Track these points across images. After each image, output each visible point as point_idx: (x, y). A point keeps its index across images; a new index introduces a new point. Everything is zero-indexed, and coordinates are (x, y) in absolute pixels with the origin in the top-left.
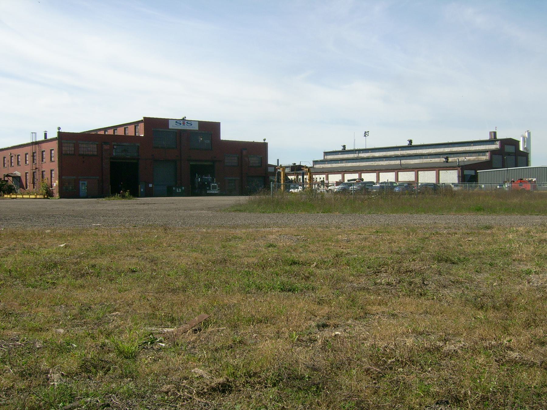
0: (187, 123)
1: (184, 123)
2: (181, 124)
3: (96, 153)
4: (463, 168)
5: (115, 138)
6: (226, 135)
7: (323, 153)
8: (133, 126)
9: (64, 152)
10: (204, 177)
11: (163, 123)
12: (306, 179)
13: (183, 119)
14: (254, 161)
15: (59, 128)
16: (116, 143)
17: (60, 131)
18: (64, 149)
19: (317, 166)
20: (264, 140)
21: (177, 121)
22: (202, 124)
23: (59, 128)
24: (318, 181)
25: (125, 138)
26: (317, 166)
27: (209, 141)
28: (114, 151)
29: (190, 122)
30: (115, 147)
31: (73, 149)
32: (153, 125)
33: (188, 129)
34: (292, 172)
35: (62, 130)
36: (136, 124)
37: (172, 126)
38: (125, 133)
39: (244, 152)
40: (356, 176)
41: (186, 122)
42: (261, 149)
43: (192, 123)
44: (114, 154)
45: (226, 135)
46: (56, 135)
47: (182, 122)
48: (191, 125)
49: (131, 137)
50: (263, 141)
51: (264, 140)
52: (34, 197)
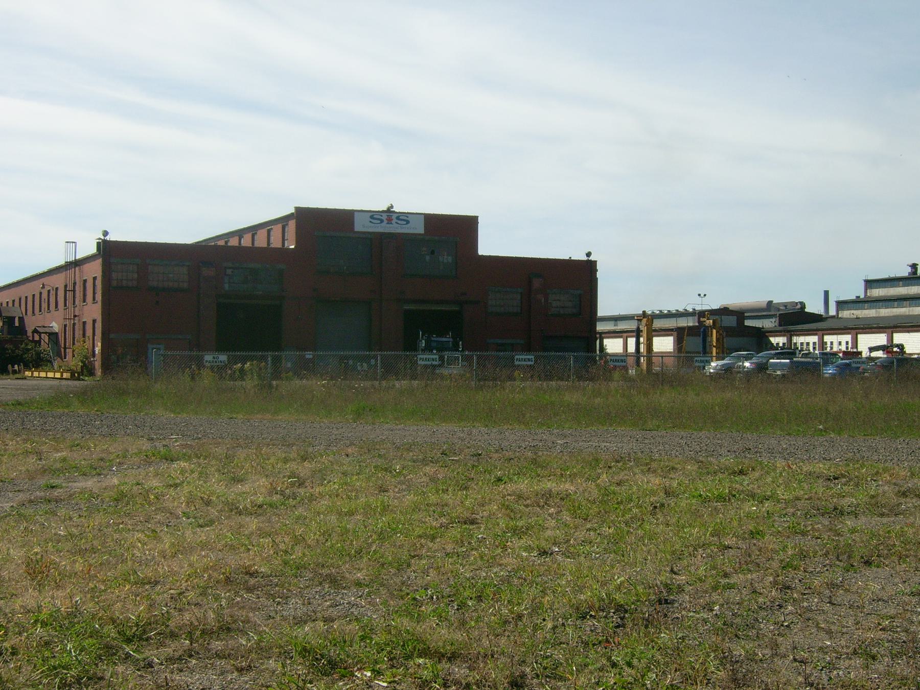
0: (398, 218)
1: (390, 220)
2: (382, 221)
3: (185, 285)
4: (680, 334)
5: (226, 249)
6: (489, 245)
7: (863, 283)
8: (280, 226)
9: (114, 283)
10: (434, 338)
11: (344, 218)
12: (795, 344)
13: (389, 211)
14: (561, 301)
15: (106, 233)
16: (230, 265)
17: (108, 238)
18: (114, 275)
19: (846, 314)
20: (589, 254)
21: (373, 215)
22: (435, 222)
23: (106, 233)
24: (835, 349)
25: (240, 249)
26: (846, 314)
27: (450, 259)
28: (226, 280)
29: (404, 218)
30: (229, 272)
31: (136, 276)
32: (310, 221)
33: (399, 231)
34: (781, 328)
35: (112, 237)
36: (283, 221)
37: (360, 226)
38: (253, 243)
39: (537, 283)
40: (881, 339)
41: (394, 216)
42: (580, 276)
43: (410, 218)
44: (227, 286)
45: (489, 245)
46: (93, 250)
47: (384, 217)
48: (408, 222)
49: (246, 249)
50: (585, 258)
51: (589, 254)
52: (58, 375)
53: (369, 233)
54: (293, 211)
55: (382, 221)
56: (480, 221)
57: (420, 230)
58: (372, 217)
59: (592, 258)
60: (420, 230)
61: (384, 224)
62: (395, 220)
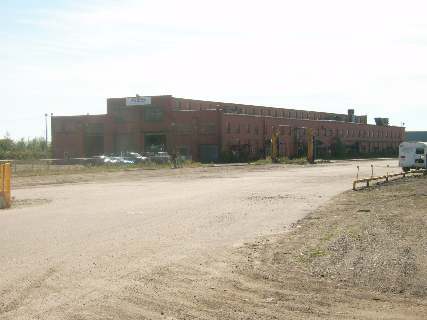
0: (141, 99)
1: (138, 100)
2: (136, 101)
11: (122, 101)
15: (52, 114)
21: (133, 99)
23: (52, 114)
29: (143, 99)
32: (114, 104)
45: (407, 130)
48: (145, 100)
53: (117, 182)
54: (102, 110)
55: (136, 101)
56: (59, 114)
57: (149, 103)
58: (132, 100)
59: (404, 126)
60: (149, 103)
61: (137, 102)
62: (140, 100)
